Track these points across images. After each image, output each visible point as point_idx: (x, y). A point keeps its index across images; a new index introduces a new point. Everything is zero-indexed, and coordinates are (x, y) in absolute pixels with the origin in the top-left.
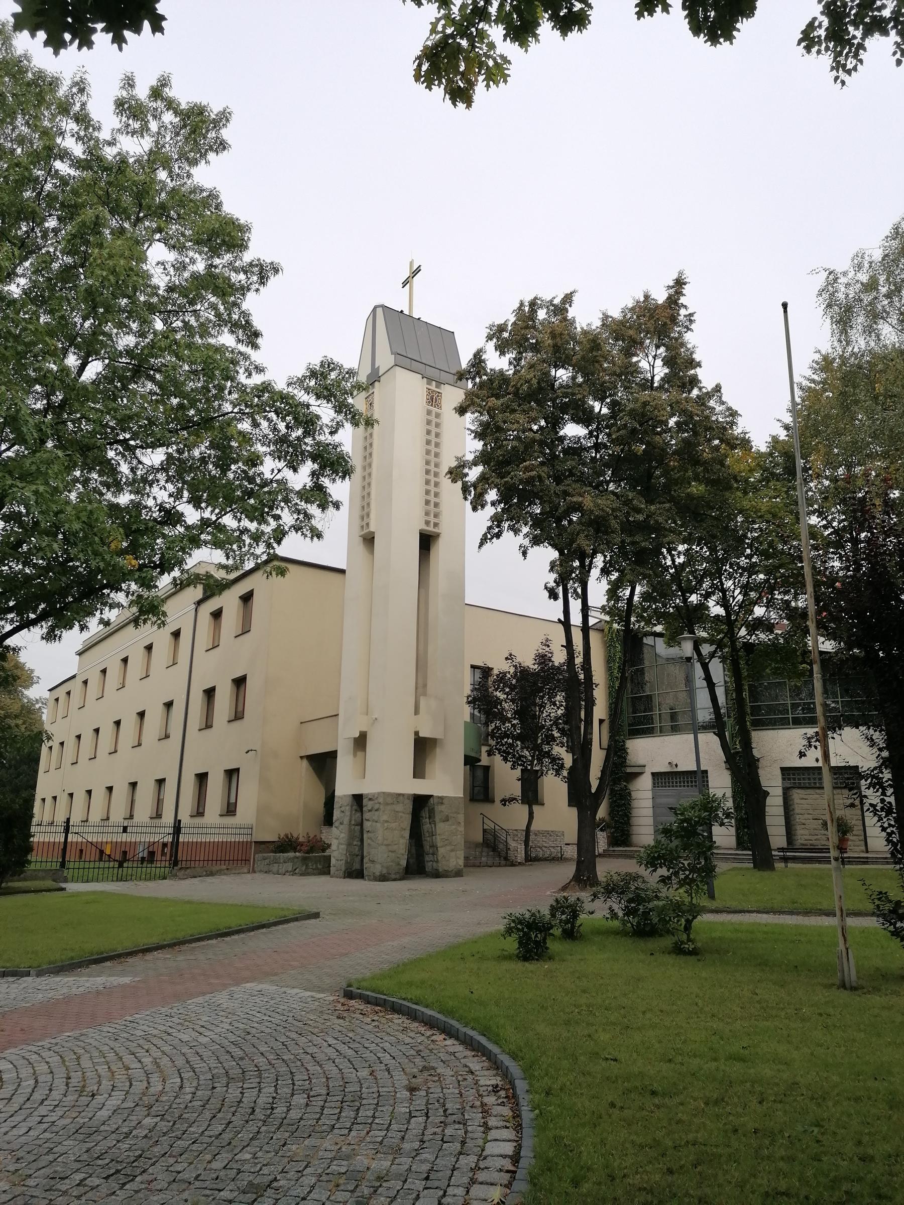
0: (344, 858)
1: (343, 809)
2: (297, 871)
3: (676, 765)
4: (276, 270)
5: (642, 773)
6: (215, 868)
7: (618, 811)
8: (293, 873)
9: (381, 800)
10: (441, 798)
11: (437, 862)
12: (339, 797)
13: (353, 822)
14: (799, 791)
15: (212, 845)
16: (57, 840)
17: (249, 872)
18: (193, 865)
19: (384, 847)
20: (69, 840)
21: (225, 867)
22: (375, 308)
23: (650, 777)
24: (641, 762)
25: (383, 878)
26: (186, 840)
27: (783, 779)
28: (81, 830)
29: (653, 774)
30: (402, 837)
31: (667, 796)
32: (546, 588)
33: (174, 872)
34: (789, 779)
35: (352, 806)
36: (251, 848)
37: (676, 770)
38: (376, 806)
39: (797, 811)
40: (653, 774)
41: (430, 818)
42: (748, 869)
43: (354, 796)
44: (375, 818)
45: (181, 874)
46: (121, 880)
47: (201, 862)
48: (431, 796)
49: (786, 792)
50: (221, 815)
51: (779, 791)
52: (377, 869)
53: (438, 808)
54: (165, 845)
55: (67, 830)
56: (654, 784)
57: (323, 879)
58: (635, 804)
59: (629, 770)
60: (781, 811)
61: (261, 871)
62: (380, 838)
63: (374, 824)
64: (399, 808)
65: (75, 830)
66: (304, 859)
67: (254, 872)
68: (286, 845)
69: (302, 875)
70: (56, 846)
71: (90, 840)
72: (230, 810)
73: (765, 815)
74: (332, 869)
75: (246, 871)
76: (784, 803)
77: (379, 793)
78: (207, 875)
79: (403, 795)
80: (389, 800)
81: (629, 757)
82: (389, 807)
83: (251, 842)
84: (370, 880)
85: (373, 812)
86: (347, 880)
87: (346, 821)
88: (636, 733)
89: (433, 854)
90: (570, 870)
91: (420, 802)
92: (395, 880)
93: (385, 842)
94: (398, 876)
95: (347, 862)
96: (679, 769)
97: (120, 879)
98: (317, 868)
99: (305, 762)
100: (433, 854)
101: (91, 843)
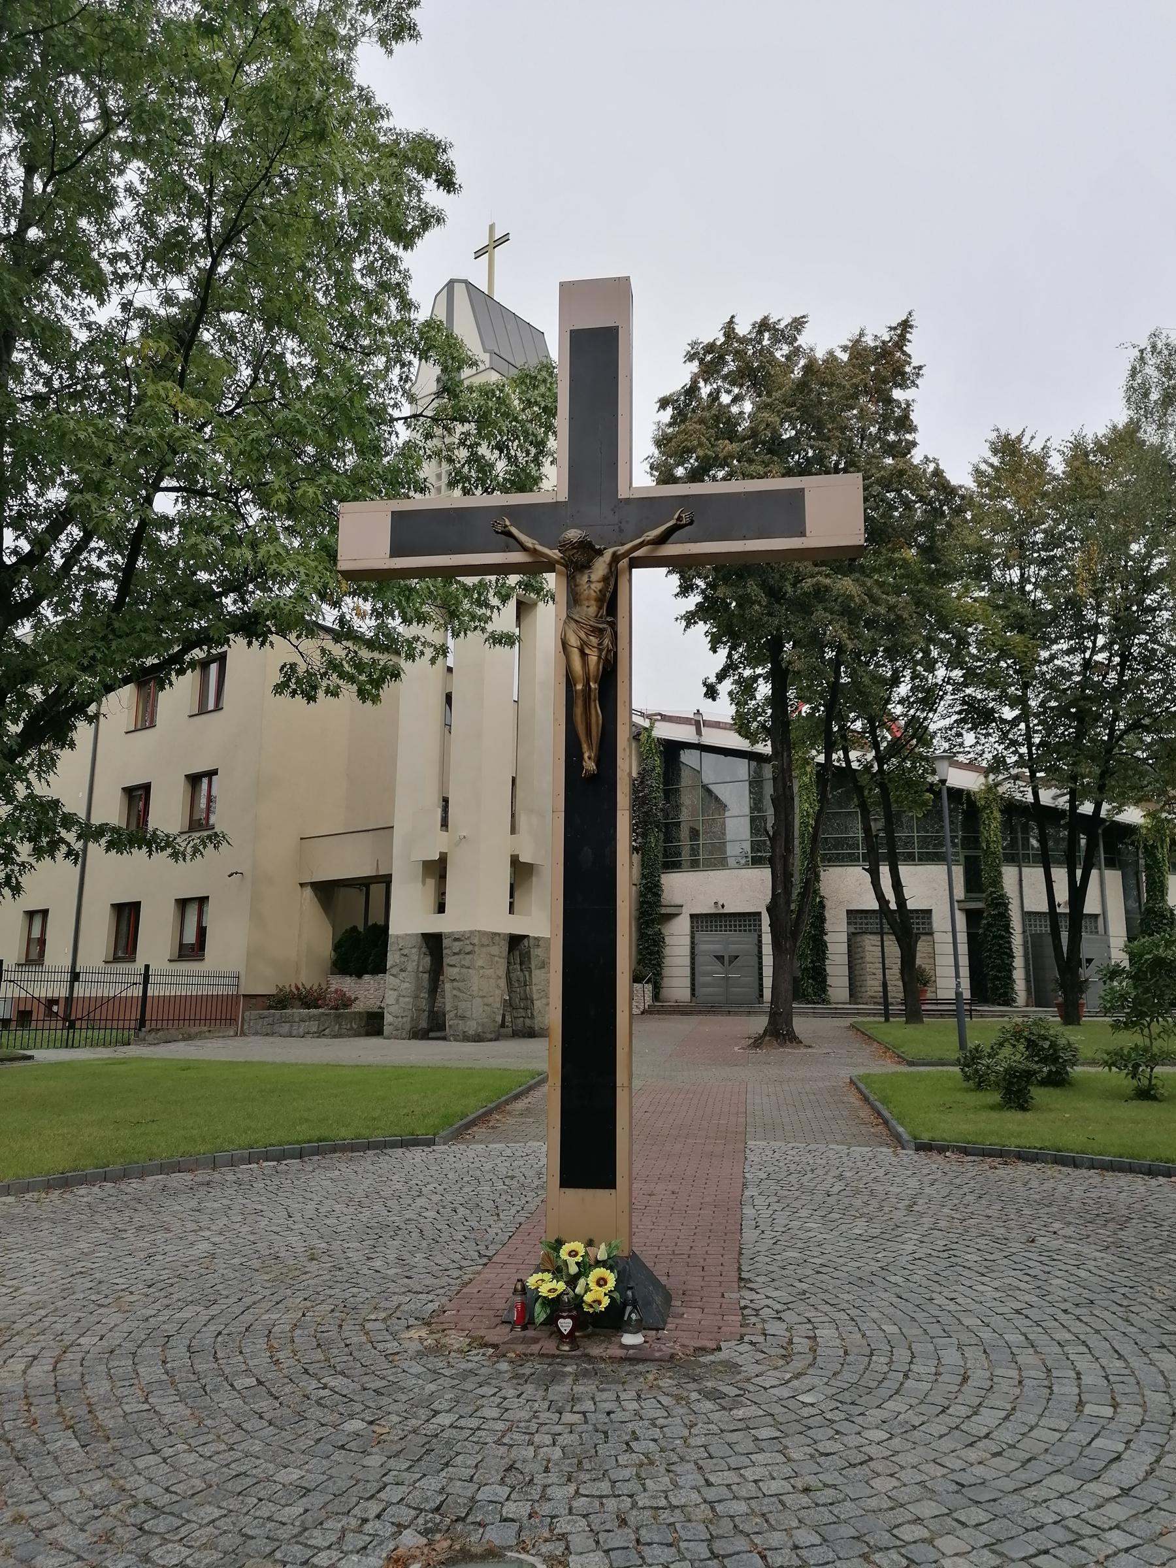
0: (409, 1014)
1: (405, 952)
2: (327, 1032)
3: (723, 906)
4: (438, 220)
5: (678, 915)
6: (194, 1030)
7: (650, 960)
8: (320, 1034)
9: (476, 941)
10: (537, 939)
11: (532, 1017)
12: (397, 937)
13: (421, 969)
14: (871, 937)
15: (178, 1000)
16: (135, 995)
17: (236, 1035)
18: (165, 1026)
19: (479, 999)
20: (150, 993)
21: (206, 1029)
22: (451, 284)
23: (688, 918)
24: (678, 902)
25: (478, 1038)
26: (156, 994)
27: (849, 923)
28: (17, 976)
29: (692, 916)
30: (498, 987)
31: (713, 942)
32: (705, 684)
33: (142, 1035)
34: (856, 923)
35: (420, 948)
36: (238, 1004)
37: (721, 911)
38: (469, 948)
39: (868, 959)
40: (692, 916)
41: (521, 964)
42: (880, 1022)
43: (426, 936)
44: (467, 963)
45: (150, 1038)
46: (72, 1047)
47: (103, 1022)
48: (527, 936)
49: (851, 936)
50: (170, 961)
51: (844, 938)
52: (472, 1027)
53: (535, 952)
54: (53, 1001)
55: (75, 976)
56: (692, 927)
57: (374, 1041)
58: (667, 951)
59: (664, 910)
60: (845, 959)
61: (256, 1034)
62: (475, 988)
63: (464, 970)
64: (495, 950)
65: (11, 976)
66: (338, 1016)
67: (243, 1034)
68: (280, 1001)
69: (335, 1037)
70: (135, 1001)
71: (36, 995)
72: (192, 951)
73: (970, 966)
74: (387, 1029)
75: (232, 1033)
76: (849, 951)
77: (472, 932)
78: (184, 1040)
79: (499, 934)
80: (485, 941)
81: (664, 895)
82: (484, 950)
83: (237, 996)
84: (456, 1040)
85: (461, 956)
86: (414, 1042)
87: (411, 966)
88: (673, 865)
89: (526, 1009)
90: (760, 1023)
91: (515, 941)
92: (491, 1040)
93: (481, 993)
94: (492, 1036)
95: (412, 1019)
96: (726, 911)
97: (68, 1044)
98: (351, 1029)
99: (308, 891)
100: (526, 1009)
101: (39, 999)
